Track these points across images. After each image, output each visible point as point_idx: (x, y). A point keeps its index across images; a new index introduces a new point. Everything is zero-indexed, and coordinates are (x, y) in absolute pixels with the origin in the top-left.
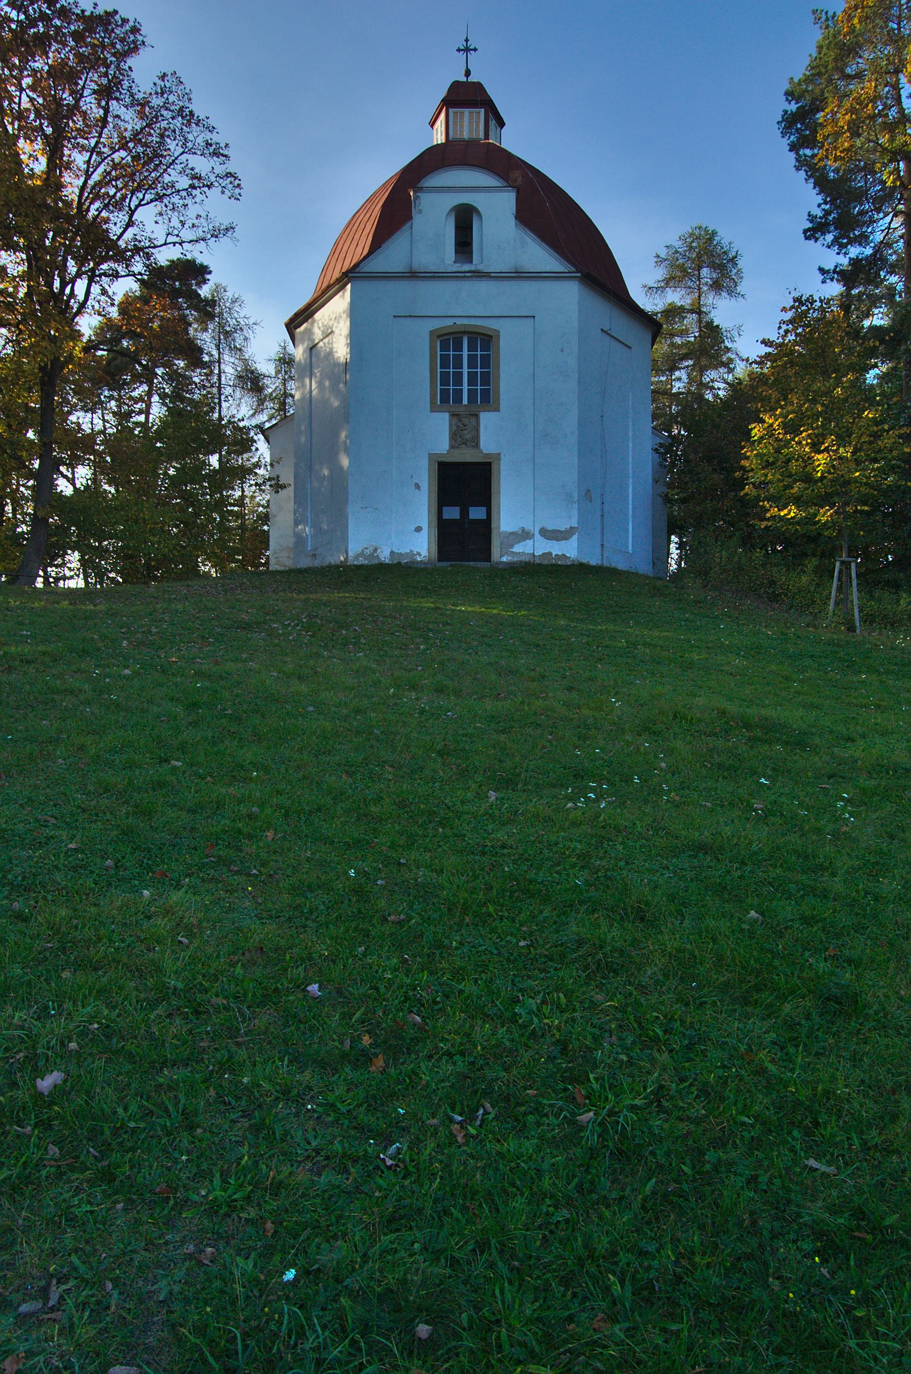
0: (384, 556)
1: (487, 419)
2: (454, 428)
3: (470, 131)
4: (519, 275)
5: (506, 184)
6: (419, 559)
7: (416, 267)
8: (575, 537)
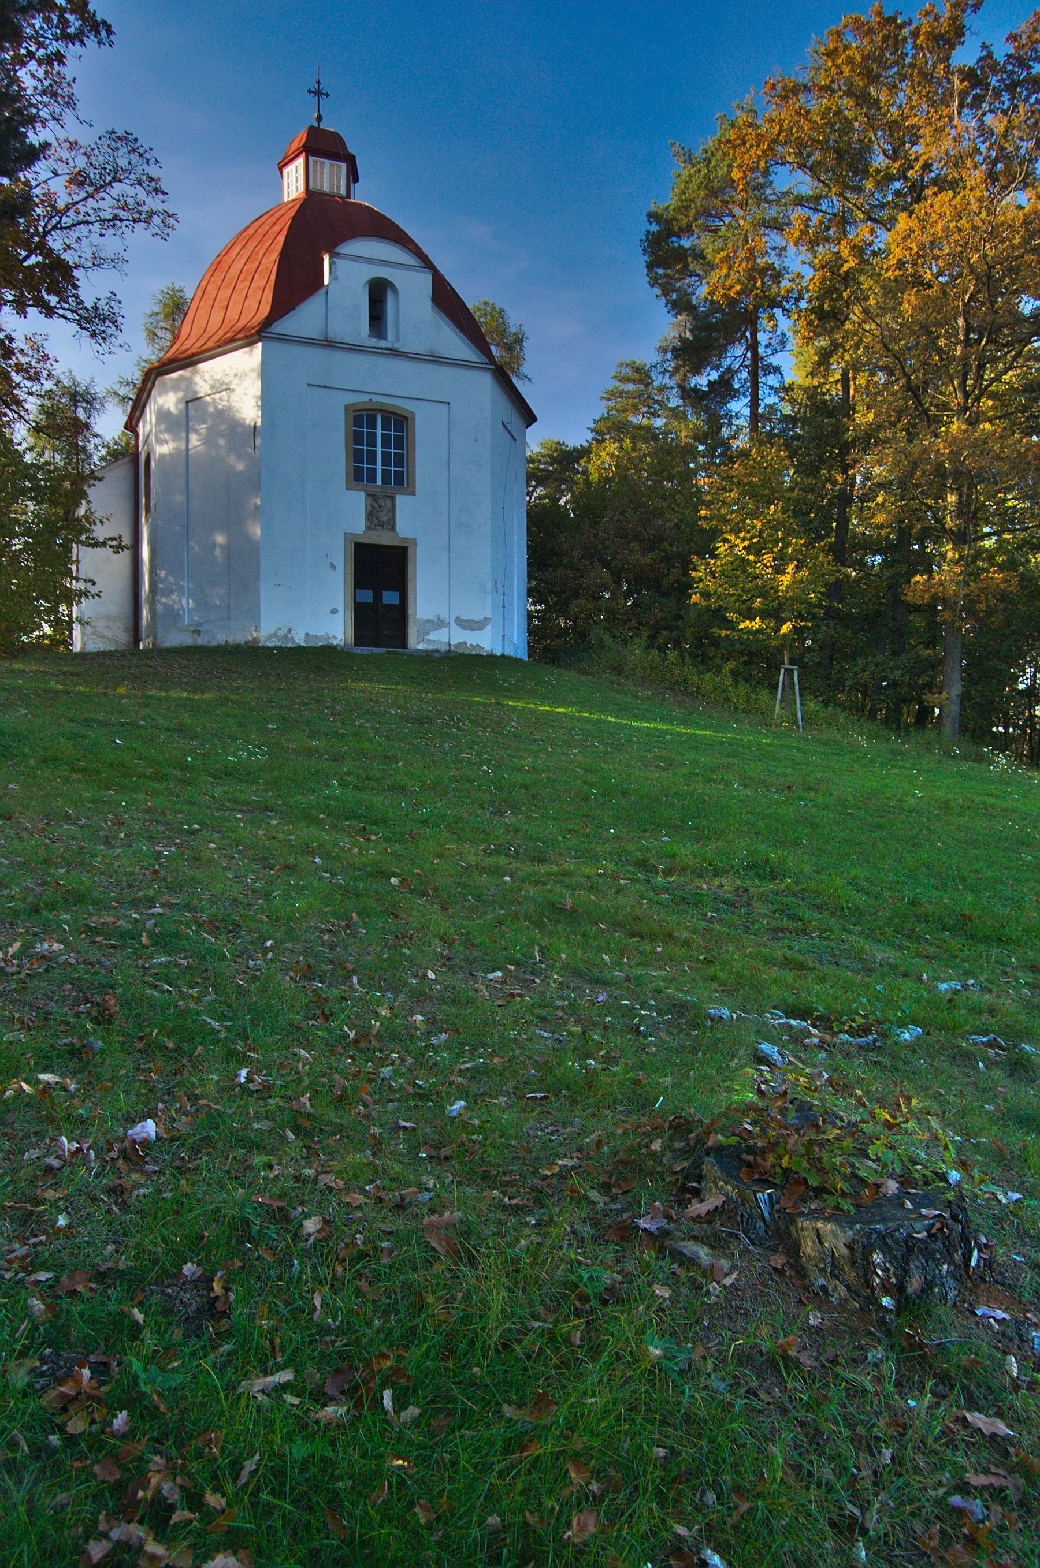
0: (299, 638)
1: (402, 502)
2: (370, 509)
3: (332, 187)
4: (435, 359)
5: (423, 265)
6: (335, 643)
7: (331, 336)
8: (489, 627)
